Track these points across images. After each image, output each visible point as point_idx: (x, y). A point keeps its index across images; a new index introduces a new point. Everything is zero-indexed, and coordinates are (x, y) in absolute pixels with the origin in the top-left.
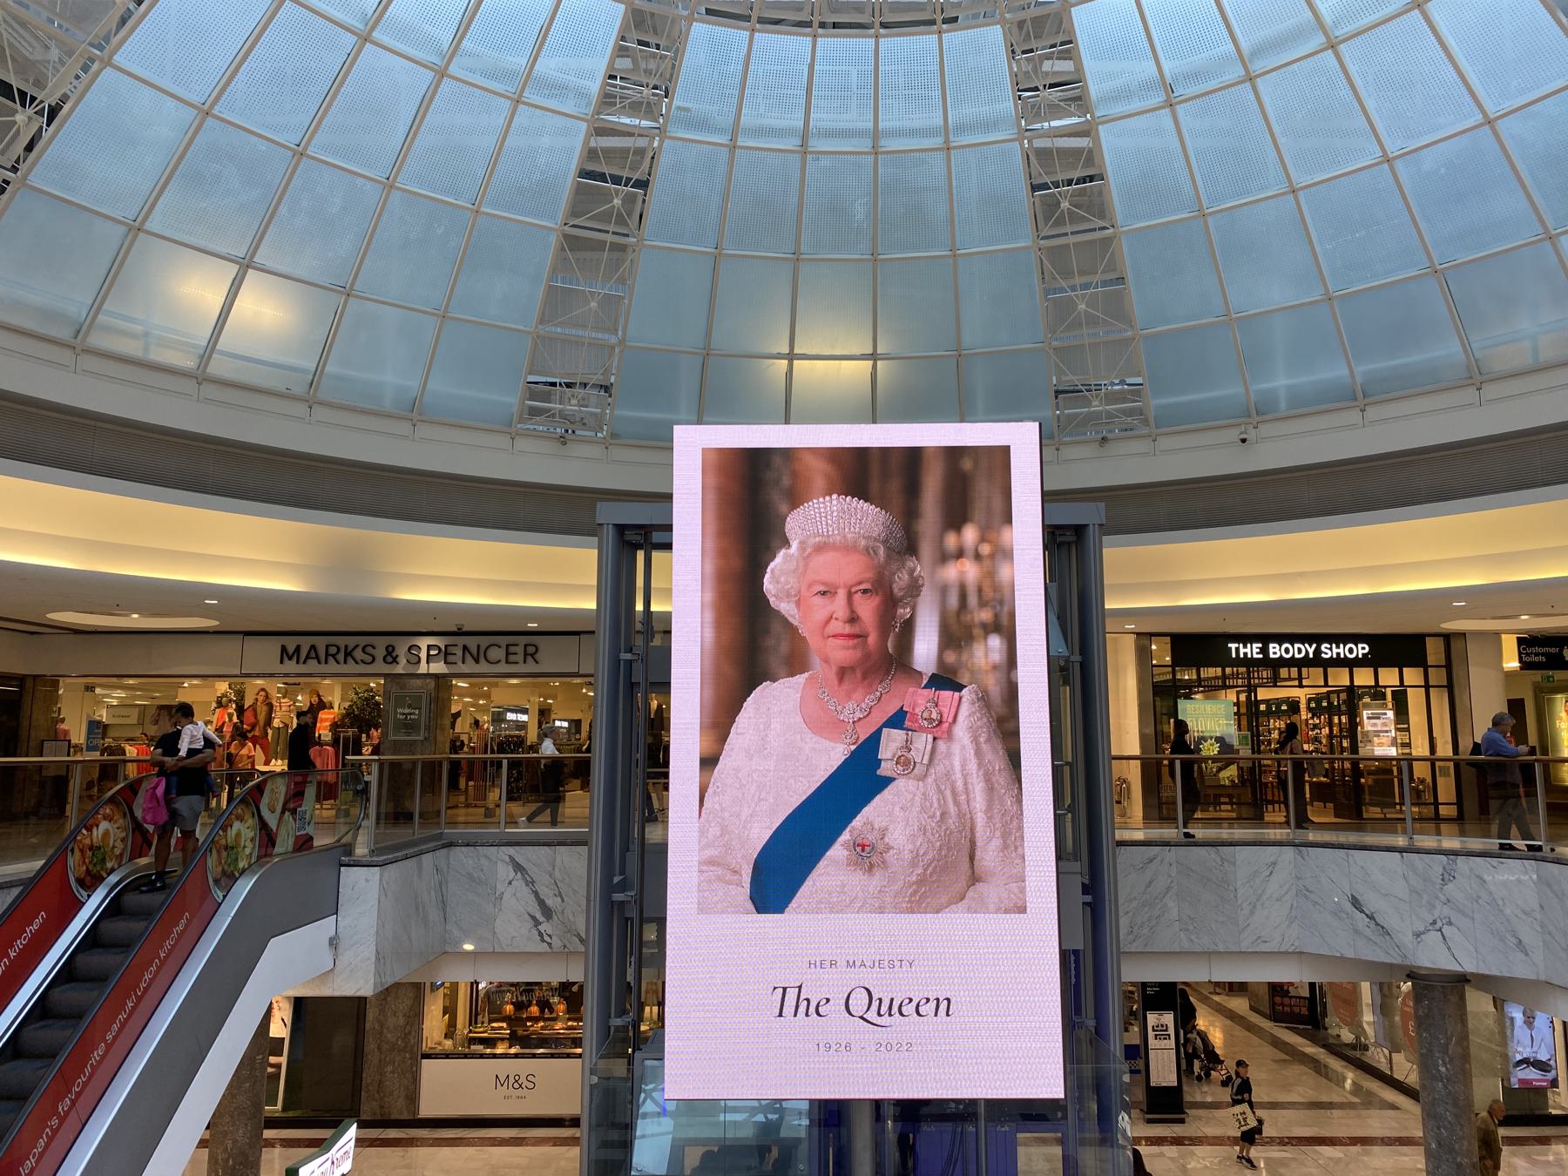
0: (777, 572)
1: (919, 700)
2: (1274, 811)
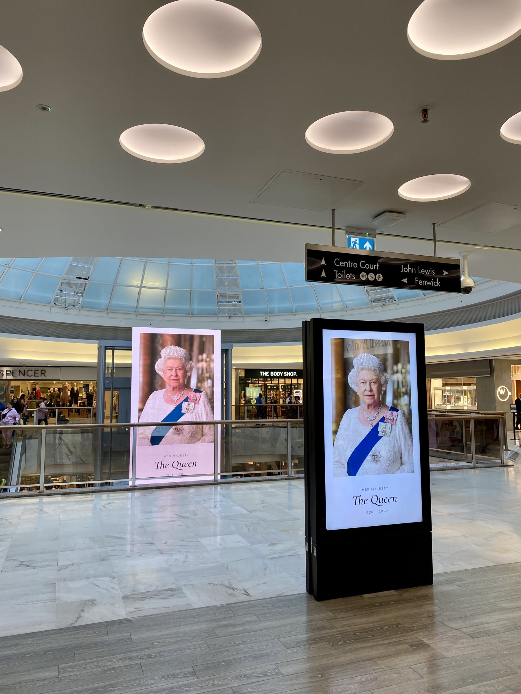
0: (158, 364)
1: (192, 395)
2: (470, 444)
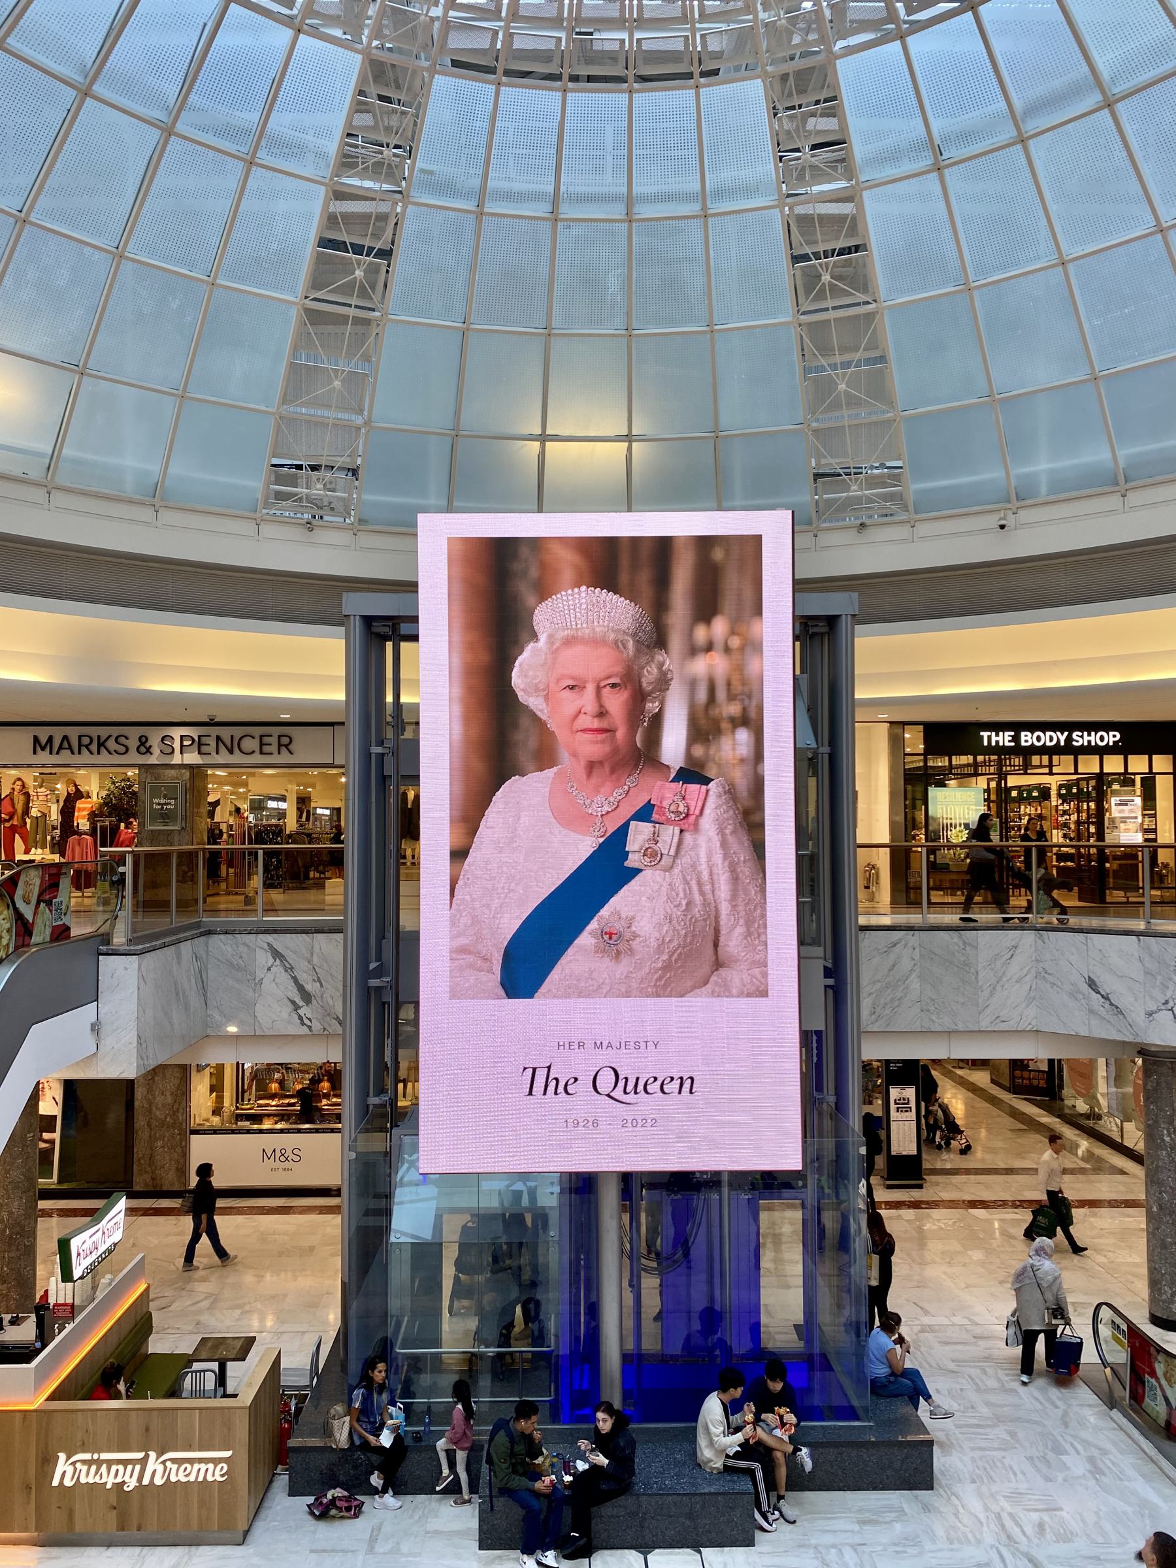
1: (667, 793)
